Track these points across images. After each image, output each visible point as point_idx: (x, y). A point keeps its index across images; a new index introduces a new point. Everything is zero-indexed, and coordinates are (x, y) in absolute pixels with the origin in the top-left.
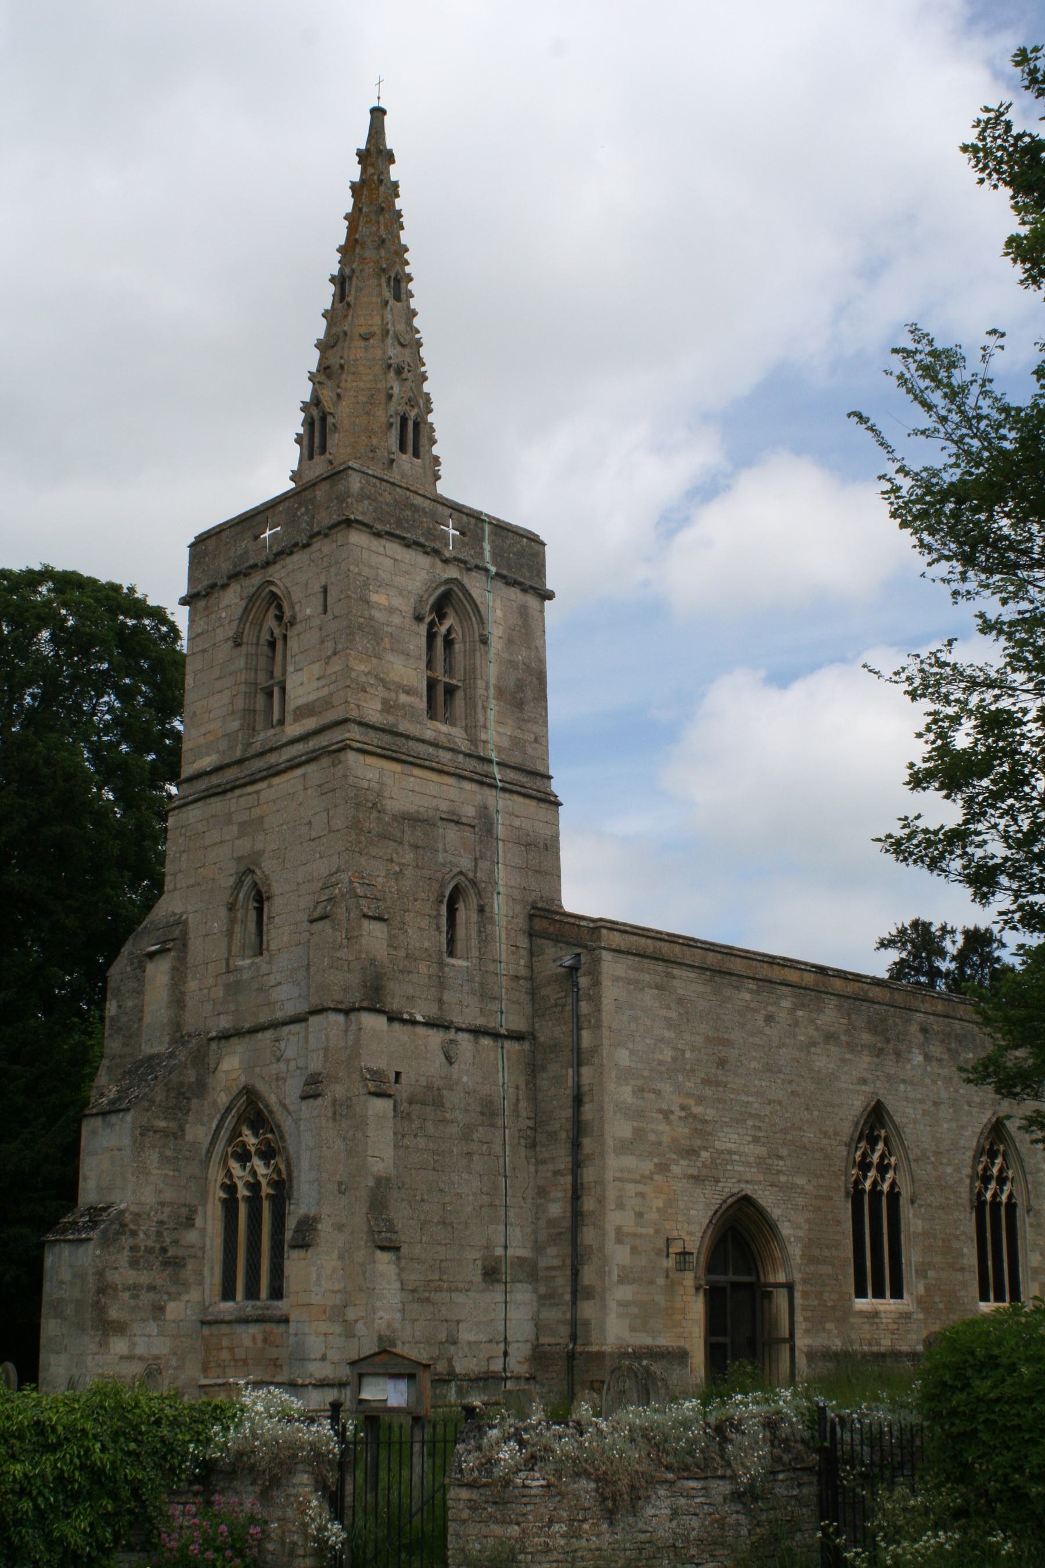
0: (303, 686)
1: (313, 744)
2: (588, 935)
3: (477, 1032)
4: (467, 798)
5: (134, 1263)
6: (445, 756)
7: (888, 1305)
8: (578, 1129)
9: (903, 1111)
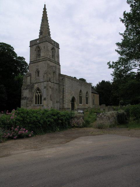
0: (42, 54)
1: (43, 59)
2: (64, 76)
3: (56, 83)
4: (55, 65)
5: (29, 101)
6: (53, 61)
7: (81, 104)
8: (63, 91)
9: (82, 91)
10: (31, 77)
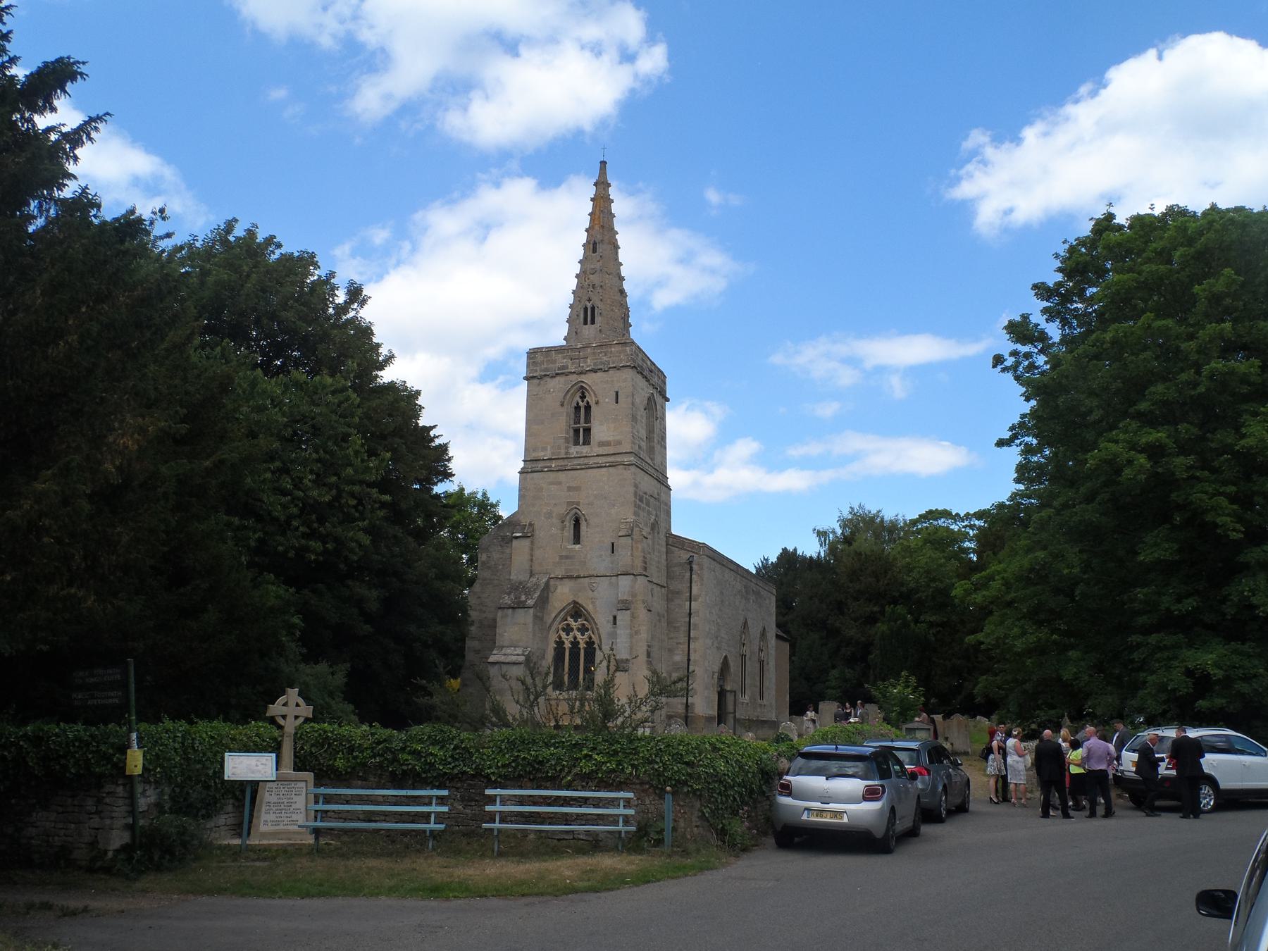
0: (601, 431)
10: (532, 543)
